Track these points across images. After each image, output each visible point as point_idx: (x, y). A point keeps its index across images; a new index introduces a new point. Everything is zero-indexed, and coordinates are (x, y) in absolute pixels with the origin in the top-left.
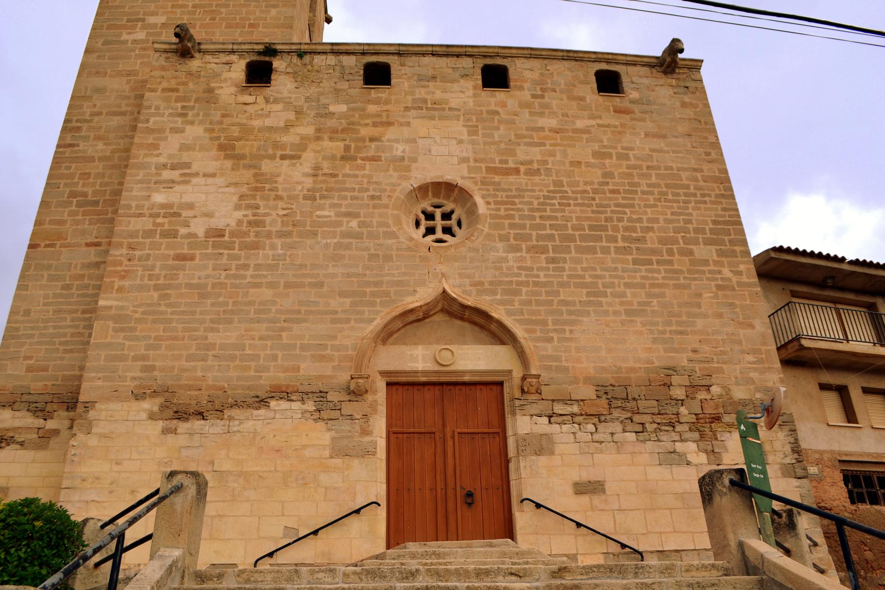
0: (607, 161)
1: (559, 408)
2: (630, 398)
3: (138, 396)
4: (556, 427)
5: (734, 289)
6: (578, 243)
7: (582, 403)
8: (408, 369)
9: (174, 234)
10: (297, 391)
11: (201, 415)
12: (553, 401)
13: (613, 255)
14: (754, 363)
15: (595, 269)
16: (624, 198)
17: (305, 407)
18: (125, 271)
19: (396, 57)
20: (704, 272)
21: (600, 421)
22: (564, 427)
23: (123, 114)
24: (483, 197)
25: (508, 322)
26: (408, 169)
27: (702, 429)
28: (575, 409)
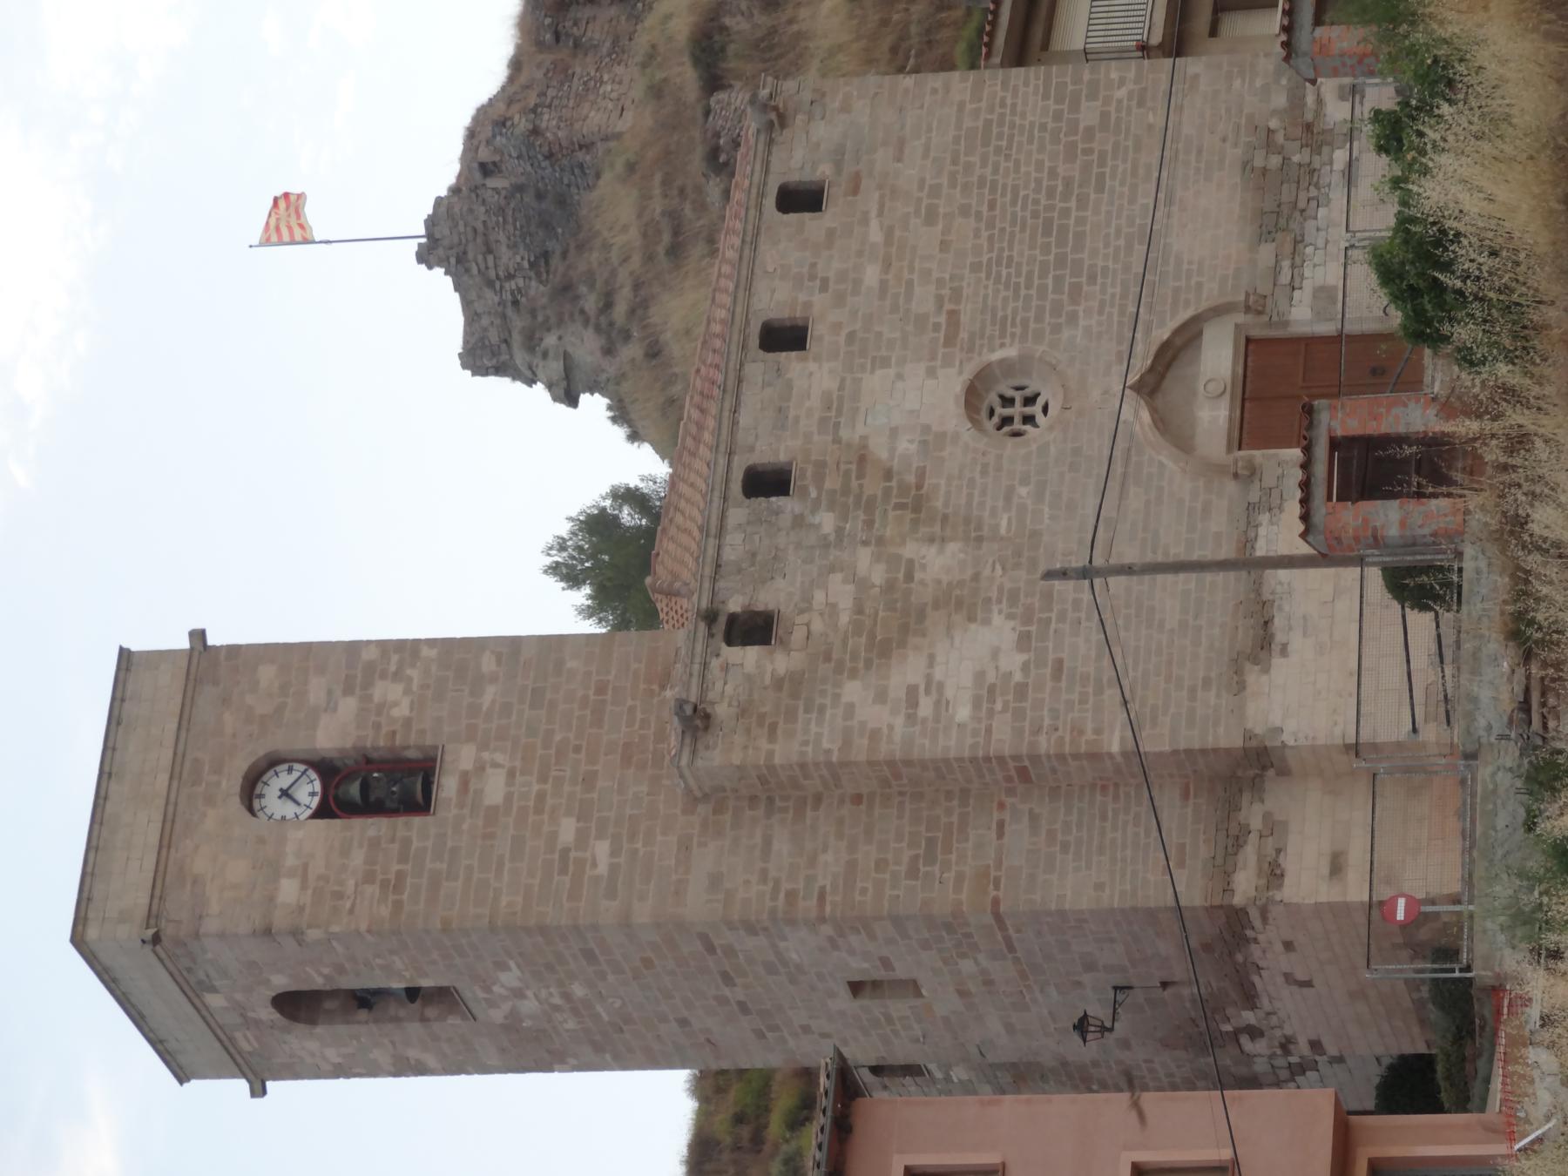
0: (941, 210)
1: (1285, 278)
2: (1277, 210)
3: (1242, 686)
4: (1307, 284)
5: (1145, 89)
6: (1069, 250)
7: (1280, 257)
8: (1227, 426)
9: (1021, 690)
10: (1246, 532)
11: (1266, 623)
12: (1275, 285)
13: (1089, 213)
14: (1244, 81)
15: (1108, 235)
16: (1003, 195)
17: (1265, 523)
18: (1072, 731)
19: (736, 458)
20: (1118, 119)
21: (1302, 241)
22: (1306, 275)
23: (768, 841)
24: (992, 350)
25: (1172, 324)
26: (941, 436)
27: (1319, 143)
28: (1286, 264)
